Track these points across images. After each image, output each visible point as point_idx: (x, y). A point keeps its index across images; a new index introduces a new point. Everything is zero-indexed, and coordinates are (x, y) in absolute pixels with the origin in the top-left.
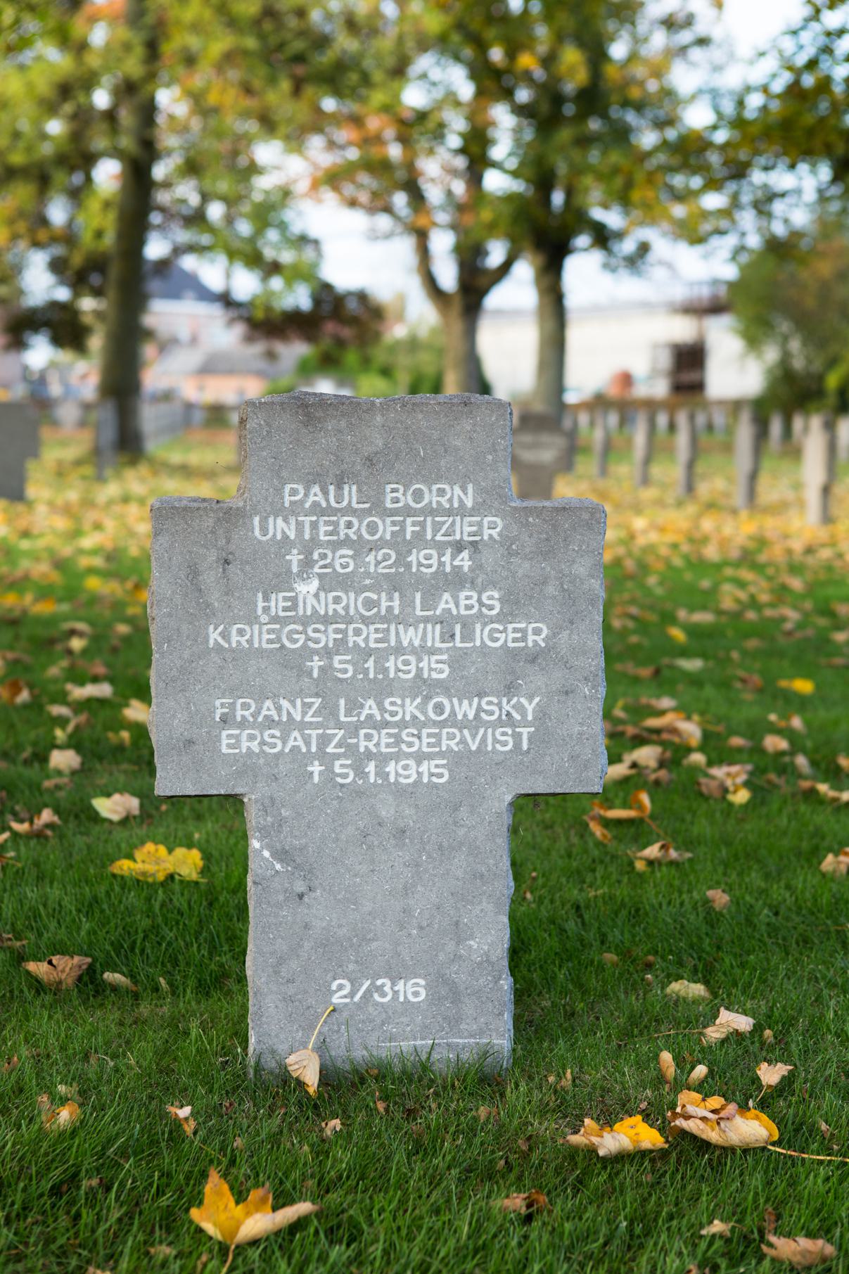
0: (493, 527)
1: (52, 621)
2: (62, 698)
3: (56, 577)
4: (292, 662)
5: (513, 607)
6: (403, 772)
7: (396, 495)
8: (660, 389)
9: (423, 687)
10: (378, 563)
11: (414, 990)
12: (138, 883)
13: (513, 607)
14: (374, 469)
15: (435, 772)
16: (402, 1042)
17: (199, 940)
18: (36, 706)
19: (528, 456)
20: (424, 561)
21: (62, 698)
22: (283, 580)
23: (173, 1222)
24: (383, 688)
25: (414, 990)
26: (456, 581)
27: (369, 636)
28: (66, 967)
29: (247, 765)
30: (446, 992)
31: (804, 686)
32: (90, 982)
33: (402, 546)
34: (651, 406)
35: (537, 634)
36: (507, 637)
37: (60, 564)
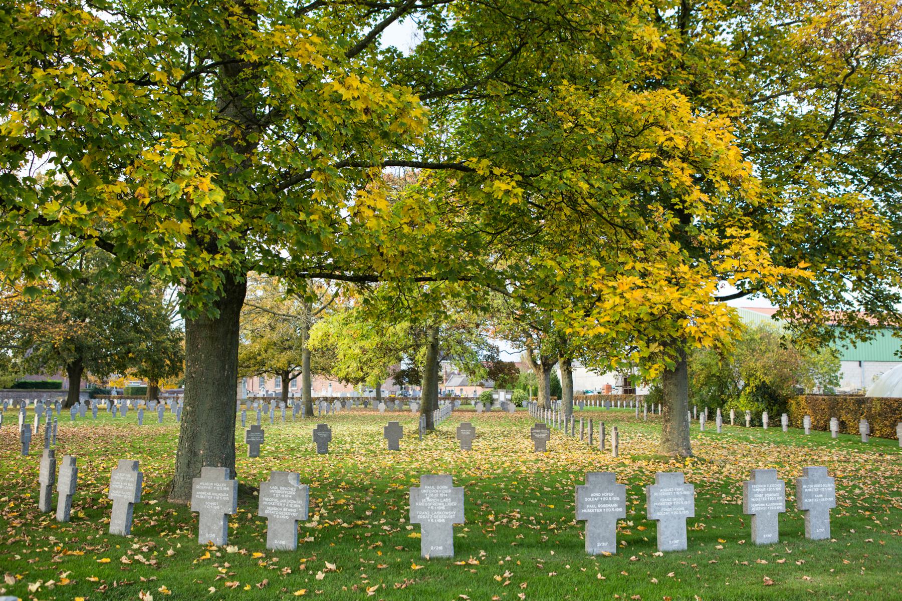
0: (450, 491)
1: (402, 491)
2: (403, 509)
3: (405, 478)
4: (426, 507)
5: (452, 501)
6: (440, 521)
7: (438, 487)
8: (620, 392)
9: (442, 510)
10: (437, 495)
11: (441, 548)
12: (412, 538)
13: (452, 501)
14: (436, 484)
15: (443, 521)
16: (440, 555)
17: (416, 545)
18: (398, 510)
19: (538, 436)
20: (442, 495)
21: (403, 509)
22: (425, 497)
23: (410, 568)
24: (437, 511)
25: (441, 548)
26: (445, 497)
27: (435, 504)
28: (400, 547)
29: (421, 520)
30: (445, 548)
31: (552, 506)
32: (403, 549)
33: (439, 493)
34: (616, 397)
35: (455, 504)
36: (452, 504)
37: (406, 474)
